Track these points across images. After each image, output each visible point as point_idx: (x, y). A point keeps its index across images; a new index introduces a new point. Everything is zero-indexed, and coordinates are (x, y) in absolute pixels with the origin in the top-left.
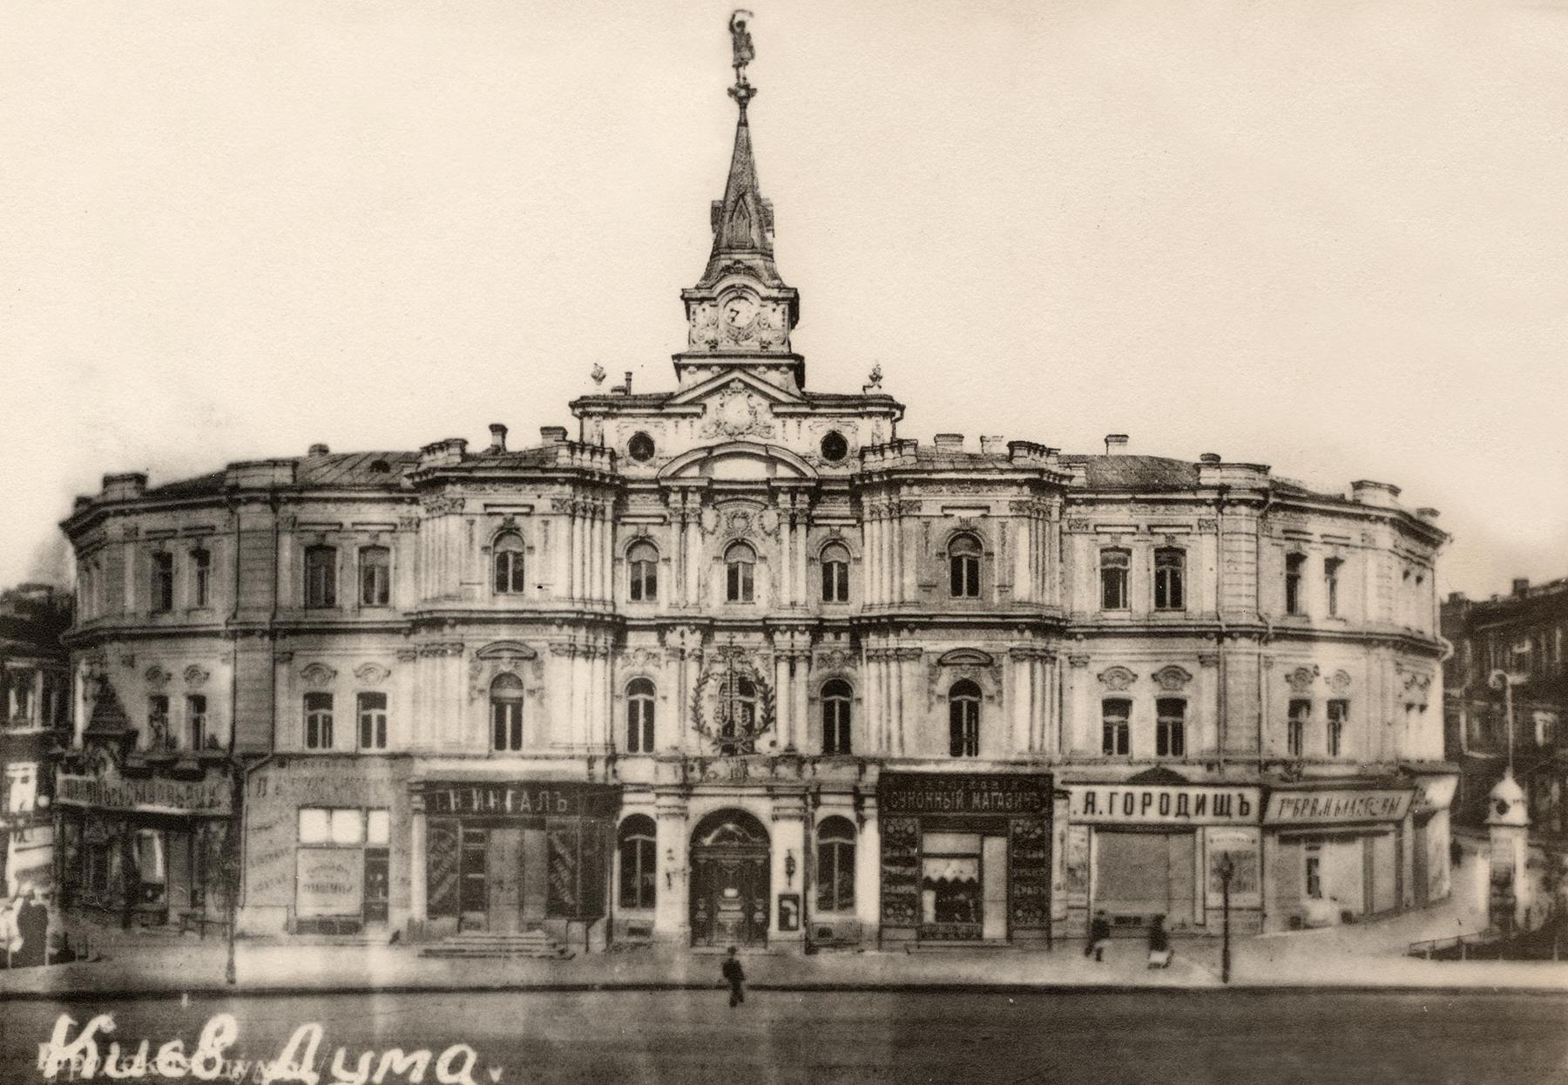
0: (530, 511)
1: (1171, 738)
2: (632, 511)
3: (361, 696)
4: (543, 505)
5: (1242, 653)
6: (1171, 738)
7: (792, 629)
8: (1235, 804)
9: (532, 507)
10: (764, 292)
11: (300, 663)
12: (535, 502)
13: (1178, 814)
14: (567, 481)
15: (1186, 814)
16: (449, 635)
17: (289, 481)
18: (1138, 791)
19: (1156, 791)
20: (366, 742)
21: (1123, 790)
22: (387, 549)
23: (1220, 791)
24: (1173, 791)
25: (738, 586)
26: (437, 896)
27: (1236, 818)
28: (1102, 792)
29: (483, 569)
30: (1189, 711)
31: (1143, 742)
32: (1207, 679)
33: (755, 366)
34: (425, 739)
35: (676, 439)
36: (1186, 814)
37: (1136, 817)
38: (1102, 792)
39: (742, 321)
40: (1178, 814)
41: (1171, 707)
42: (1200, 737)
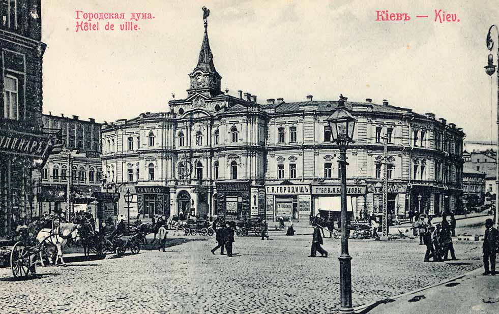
0: (238, 122)
1: (293, 173)
2: (179, 126)
3: (128, 170)
4: (157, 127)
5: (309, 154)
6: (293, 173)
7: (206, 151)
8: (304, 188)
9: (238, 121)
10: (203, 74)
11: (127, 163)
12: (239, 120)
13: (292, 192)
14: (245, 115)
15: (294, 192)
16: (223, 152)
17: (274, 112)
18: (283, 186)
19: (287, 186)
20: (292, 177)
21: (279, 186)
22: (284, 128)
23: (300, 186)
24: (291, 186)
25: (235, 138)
26: (140, 210)
27: (305, 193)
28: (275, 187)
29: (229, 137)
30: (332, 166)
31: (287, 176)
32: (300, 158)
33: (201, 91)
34: (147, 177)
35: (187, 109)
36: (294, 192)
37: (283, 193)
38: (275, 187)
39: (199, 80)
40: (292, 192)
41: (293, 166)
42: (299, 174)
